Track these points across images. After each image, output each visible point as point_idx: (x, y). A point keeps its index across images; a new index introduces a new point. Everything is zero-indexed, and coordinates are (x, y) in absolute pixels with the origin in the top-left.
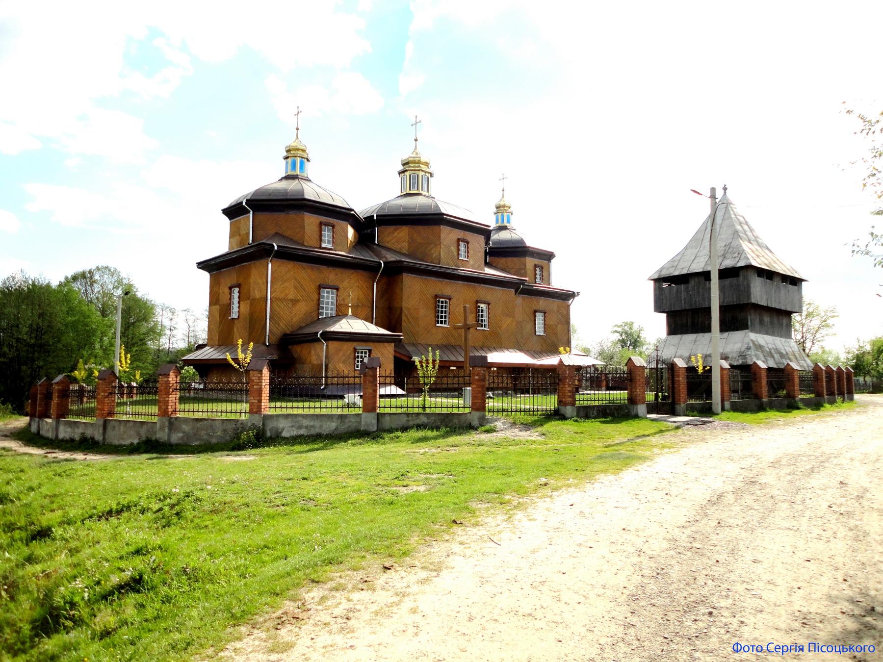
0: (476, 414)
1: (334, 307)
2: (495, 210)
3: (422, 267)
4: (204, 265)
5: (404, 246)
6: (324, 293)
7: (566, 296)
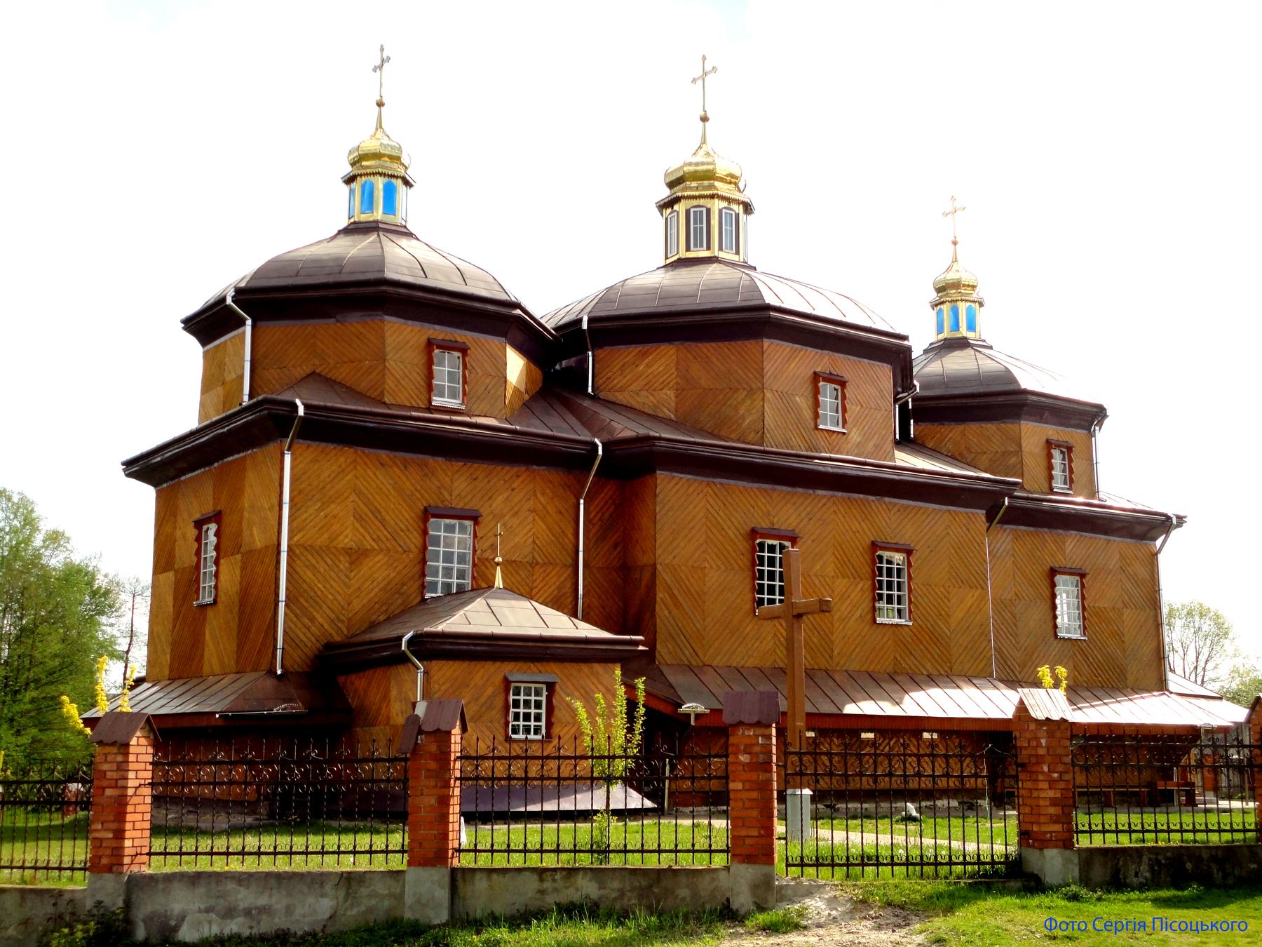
0: (747, 873)
1: (468, 567)
2: (933, 296)
3: (708, 452)
4: (140, 468)
5: (666, 400)
6: (438, 528)
7: (1149, 528)
